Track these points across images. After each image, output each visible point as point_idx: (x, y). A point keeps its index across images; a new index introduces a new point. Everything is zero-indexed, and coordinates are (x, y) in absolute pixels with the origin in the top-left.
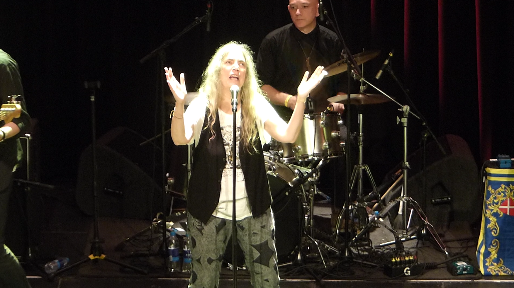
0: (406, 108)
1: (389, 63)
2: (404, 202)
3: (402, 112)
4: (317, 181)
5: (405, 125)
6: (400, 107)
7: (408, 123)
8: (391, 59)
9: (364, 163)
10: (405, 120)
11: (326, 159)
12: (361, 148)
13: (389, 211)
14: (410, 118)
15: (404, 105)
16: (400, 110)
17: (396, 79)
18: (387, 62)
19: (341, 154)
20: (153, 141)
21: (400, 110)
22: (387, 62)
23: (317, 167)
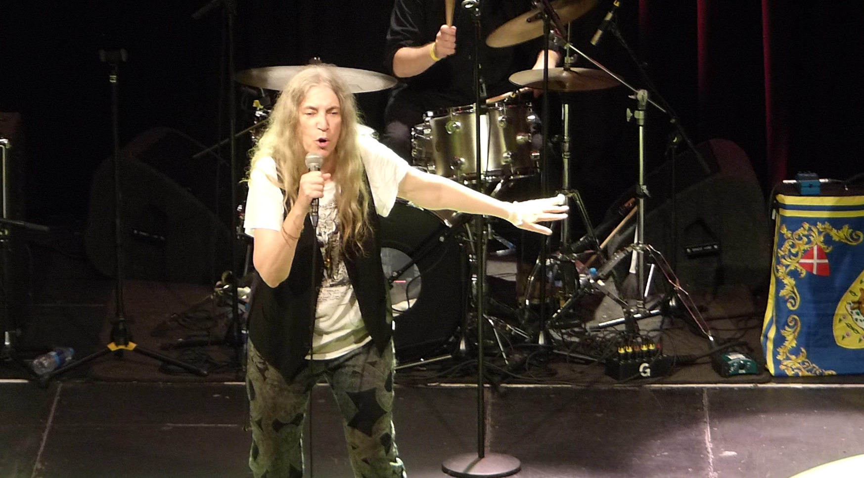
0: (642, 95)
1: (613, 19)
2: (638, 254)
3: (636, 101)
6: (633, 93)
7: (646, 119)
8: (617, 11)
9: (572, 187)
10: (640, 115)
12: (566, 161)
14: (650, 111)
15: (638, 88)
16: (632, 97)
17: (626, 46)
18: (609, 16)
19: (533, 172)
21: (632, 97)
22: (609, 16)
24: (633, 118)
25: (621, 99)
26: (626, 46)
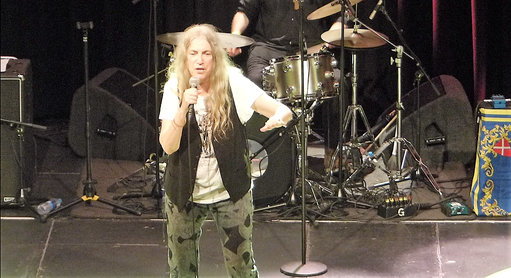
2: (398, 143)
4: (311, 122)
5: (399, 65)
6: (394, 48)
7: (402, 64)
9: (358, 103)
10: (399, 61)
11: (319, 99)
13: (383, 152)
17: (390, 20)
19: (334, 95)
20: (146, 82)
23: (311, 108)
24: (394, 63)
25: (386, 52)
26: (390, 20)
